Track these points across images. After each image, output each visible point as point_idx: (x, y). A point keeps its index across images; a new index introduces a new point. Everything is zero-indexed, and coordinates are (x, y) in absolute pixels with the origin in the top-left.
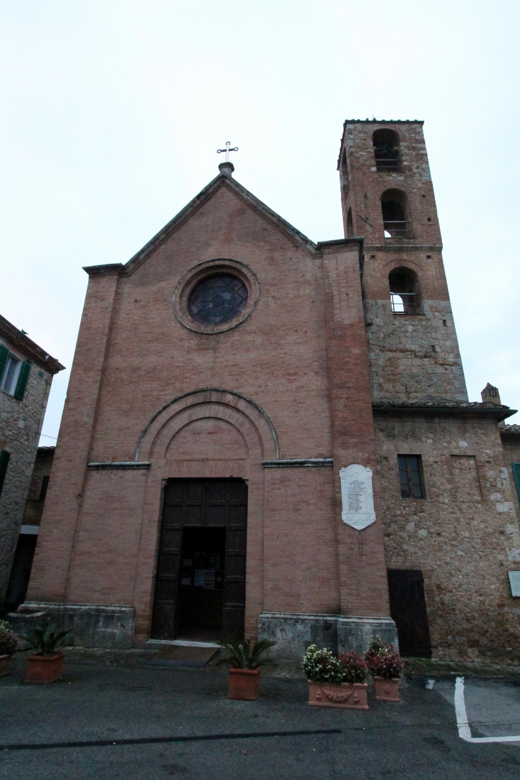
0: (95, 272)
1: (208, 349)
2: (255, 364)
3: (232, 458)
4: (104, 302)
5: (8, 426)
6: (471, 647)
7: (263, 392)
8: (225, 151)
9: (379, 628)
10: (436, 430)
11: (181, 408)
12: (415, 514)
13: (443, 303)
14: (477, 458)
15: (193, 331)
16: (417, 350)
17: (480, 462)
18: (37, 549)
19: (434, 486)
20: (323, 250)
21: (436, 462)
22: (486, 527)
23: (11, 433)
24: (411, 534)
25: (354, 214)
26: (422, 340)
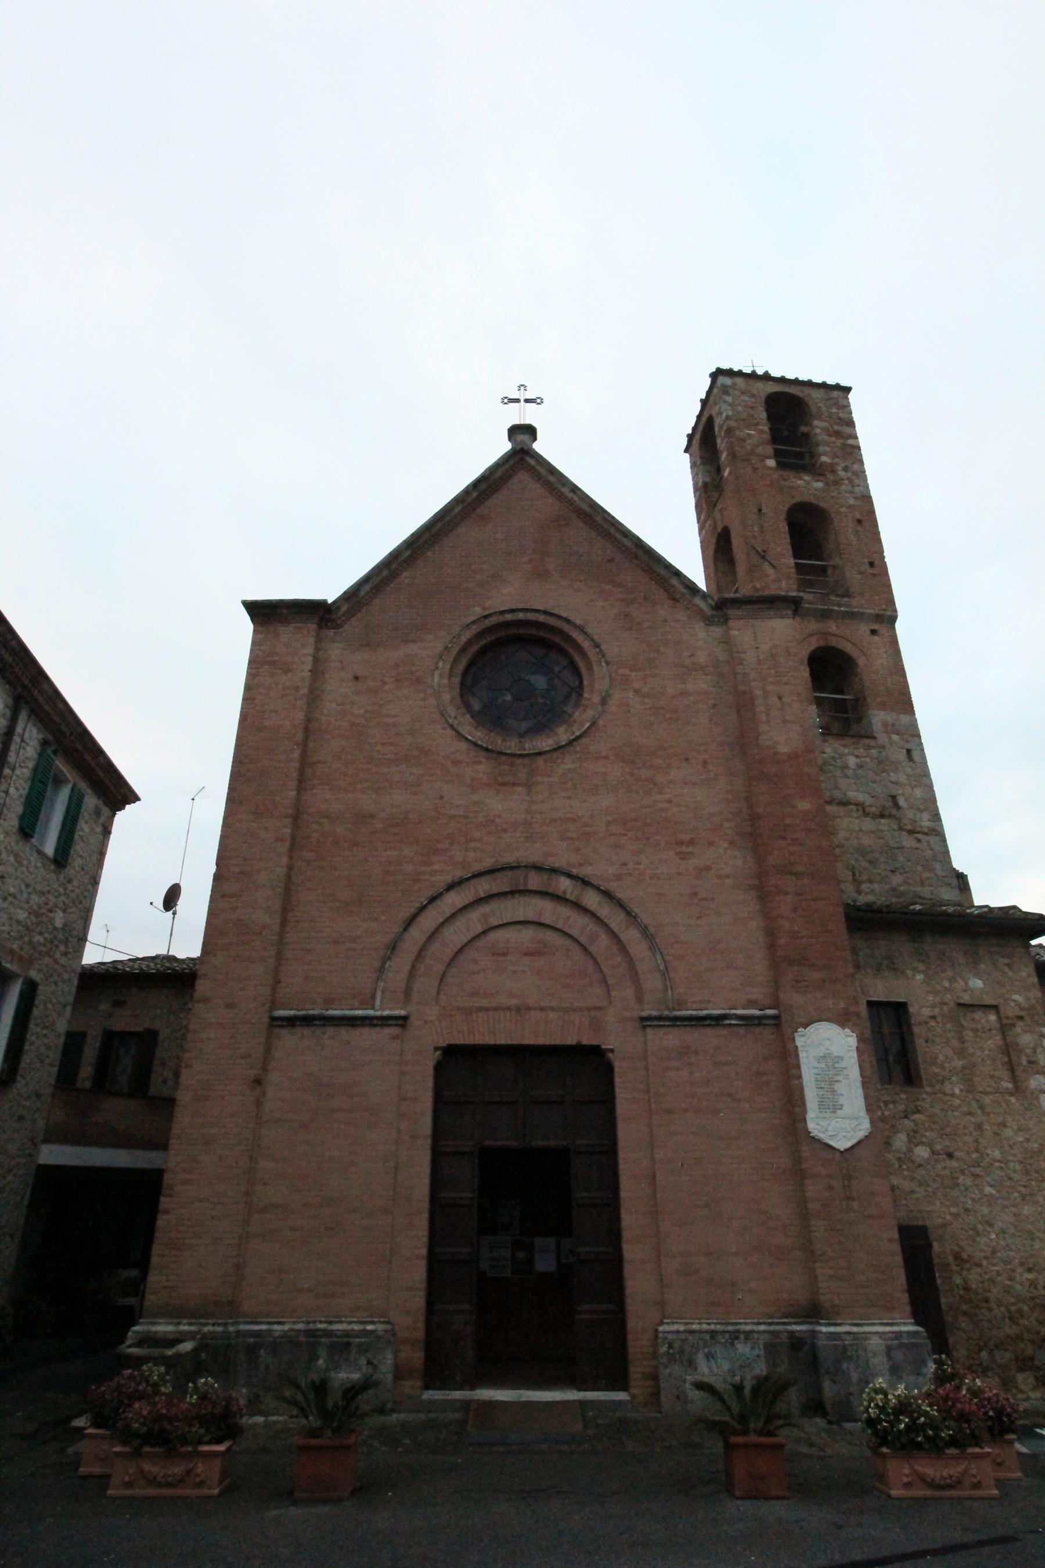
0: (264, 613)
1: (514, 784)
2: (610, 819)
3: (575, 1005)
4: (290, 675)
5: (38, 924)
6: (1021, 1370)
7: (630, 874)
8: (517, 401)
9: (896, 1342)
10: (928, 956)
11: (467, 902)
12: (906, 1117)
13: (904, 719)
14: (1002, 1008)
15: (481, 747)
16: (867, 804)
17: (1008, 1018)
18: (164, 1201)
19: (934, 1063)
20: (729, 612)
21: (934, 1017)
22: (1028, 1140)
23: (41, 939)
24: (902, 1156)
25: (736, 542)
26: (875, 785)
